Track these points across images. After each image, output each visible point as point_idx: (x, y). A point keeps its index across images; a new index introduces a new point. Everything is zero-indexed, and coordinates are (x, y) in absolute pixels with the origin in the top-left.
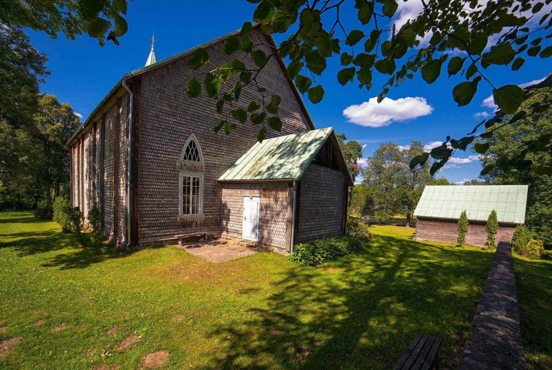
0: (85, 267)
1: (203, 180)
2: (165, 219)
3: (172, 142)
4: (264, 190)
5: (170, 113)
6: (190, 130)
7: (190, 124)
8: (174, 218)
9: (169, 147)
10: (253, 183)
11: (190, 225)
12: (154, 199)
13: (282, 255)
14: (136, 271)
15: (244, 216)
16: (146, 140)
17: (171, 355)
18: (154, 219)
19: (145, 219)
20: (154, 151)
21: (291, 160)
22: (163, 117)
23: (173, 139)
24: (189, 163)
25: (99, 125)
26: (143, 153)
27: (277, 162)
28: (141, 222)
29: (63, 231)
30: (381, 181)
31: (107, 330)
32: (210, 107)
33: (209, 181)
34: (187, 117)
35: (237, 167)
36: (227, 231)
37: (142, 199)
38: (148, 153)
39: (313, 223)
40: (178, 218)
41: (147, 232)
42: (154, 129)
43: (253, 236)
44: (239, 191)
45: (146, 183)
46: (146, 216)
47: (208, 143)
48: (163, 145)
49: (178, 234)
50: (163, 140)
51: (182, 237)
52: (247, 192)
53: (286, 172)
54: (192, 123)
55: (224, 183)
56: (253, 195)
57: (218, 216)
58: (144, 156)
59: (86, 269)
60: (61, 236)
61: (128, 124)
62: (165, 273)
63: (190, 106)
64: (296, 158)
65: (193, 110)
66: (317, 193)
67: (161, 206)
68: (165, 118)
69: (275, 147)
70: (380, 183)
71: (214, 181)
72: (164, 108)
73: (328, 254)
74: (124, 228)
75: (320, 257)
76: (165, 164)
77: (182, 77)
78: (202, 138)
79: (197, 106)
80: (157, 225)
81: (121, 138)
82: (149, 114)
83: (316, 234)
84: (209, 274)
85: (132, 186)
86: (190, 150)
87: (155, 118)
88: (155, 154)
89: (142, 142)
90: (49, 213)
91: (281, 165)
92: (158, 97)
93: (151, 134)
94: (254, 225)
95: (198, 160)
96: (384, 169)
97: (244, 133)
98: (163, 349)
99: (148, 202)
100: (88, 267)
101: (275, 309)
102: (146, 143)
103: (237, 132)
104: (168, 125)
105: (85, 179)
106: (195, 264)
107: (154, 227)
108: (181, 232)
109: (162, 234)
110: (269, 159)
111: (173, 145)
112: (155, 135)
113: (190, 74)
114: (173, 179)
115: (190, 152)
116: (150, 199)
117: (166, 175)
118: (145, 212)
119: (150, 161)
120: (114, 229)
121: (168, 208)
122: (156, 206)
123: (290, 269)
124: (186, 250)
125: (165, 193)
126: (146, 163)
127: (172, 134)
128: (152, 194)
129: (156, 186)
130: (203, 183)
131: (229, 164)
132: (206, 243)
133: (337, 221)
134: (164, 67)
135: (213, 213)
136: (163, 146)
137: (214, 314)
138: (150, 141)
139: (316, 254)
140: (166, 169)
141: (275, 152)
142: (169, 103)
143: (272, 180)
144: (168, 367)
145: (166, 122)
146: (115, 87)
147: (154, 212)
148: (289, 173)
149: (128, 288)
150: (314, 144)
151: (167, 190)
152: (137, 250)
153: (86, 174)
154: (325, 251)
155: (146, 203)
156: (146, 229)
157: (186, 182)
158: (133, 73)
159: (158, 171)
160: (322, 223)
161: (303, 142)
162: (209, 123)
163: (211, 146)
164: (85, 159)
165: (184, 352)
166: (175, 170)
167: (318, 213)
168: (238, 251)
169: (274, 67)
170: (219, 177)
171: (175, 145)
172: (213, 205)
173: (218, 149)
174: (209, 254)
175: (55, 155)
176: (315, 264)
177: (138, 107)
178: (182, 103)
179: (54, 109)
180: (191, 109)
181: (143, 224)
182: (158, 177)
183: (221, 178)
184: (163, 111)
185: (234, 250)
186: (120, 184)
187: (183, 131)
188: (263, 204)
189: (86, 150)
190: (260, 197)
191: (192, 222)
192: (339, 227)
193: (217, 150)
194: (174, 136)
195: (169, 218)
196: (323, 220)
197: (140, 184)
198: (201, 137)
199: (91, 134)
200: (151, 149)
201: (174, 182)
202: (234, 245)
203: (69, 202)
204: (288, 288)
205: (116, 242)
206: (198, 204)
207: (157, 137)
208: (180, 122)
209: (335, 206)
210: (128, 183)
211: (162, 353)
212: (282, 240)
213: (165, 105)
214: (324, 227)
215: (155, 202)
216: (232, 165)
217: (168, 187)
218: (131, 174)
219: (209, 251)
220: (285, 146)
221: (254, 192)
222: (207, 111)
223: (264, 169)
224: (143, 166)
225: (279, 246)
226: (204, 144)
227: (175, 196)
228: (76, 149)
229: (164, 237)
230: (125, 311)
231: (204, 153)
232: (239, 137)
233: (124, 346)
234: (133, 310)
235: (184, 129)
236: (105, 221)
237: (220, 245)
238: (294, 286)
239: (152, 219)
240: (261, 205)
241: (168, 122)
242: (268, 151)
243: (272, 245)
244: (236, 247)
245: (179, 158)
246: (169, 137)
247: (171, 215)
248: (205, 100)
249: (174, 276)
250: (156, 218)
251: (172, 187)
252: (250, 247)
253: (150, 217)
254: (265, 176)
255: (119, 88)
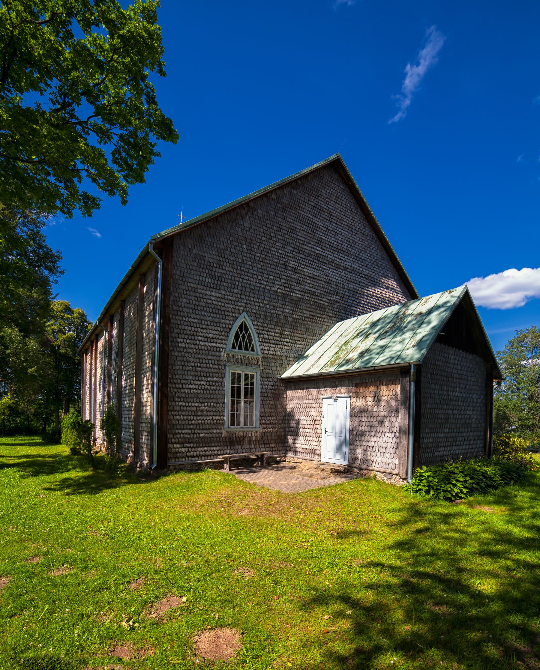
0: (96, 494)
1: (259, 378)
2: (206, 432)
3: (215, 325)
4: (357, 385)
5: (212, 285)
6: (240, 308)
7: (240, 300)
8: (218, 431)
9: (211, 331)
10: (338, 378)
11: (240, 441)
12: (190, 404)
13: (391, 484)
14: (167, 501)
15: (323, 427)
16: (179, 322)
17: (246, 637)
18: (189, 431)
19: (177, 431)
20: (190, 337)
21: (398, 339)
22: (203, 292)
23: (216, 320)
24: (240, 354)
25: (117, 317)
26: (175, 340)
27: (375, 345)
28: (172, 436)
29: (72, 453)
30: (521, 386)
31: (129, 582)
32: (267, 276)
33: (269, 380)
34: (235, 291)
35: (309, 359)
36: (295, 452)
37: (173, 404)
38: (182, 340)
39: (440, 435)
40: (224, 432)
41: (180, 449)
42: (190, 307)
43: (338, 456)
44: (314, 392)
45: (179, 381)
46: (178, 427)
47: (266, 325)
48: (203, 328)
49: (224, 454)
50: (203, 322)
51: (230, 458)
52: (328, 392)
53: (393, 356)
54: (243, 299)
55: (291, 382)
56: (338, 395)
57: (281, 430)
58: (177, 345)
59: (99, 496)
60: (68, 458)
61: (155, 302)
62: (211, 505)
63: (239, 276)
64: (408, 335)
65: (244, 281)
66: (445, 388)
67: (200, 413)
68: (205, 292)
69: (368, 326)
70: (518, 389)
71: (275, 380)
72: (204, 279)
73: (473, 483)
74: (147, 445)
75: (461, 486)
76: (206, 355)
77: (228, 237)
78: (258, 319)
79: (249, 275)
80: (194, 441)
81: (145, 325)
82: (184, 287)
83: (445, 453)
84: (279, 509)
85: (160, 384)
86: (241, 336)
87: (191, 293)
88: (192, 342)
89: (174, 325)
90: (57, 436)
91: (383, 348)
92: (196, 265)
93: (186, 314)
94: (340, 440)
95: (253, 350)
96: (524, 367)
97: (317, 311)
98: (229, 625)
99: (182, 408)
100: (101, 494)
101: (413, 565)
102: (180, 326)
103: (306, 310)
104: (209, 301)
105: (98, 389)
106: (254, 495)
107: (190, 443)
108: (228, 451)
109: (201, 453)
110: (362, 341)
111: (216, 328)
112: (192, 316)
113: (238, 233)
114: (217, 375)
115: (241, 338)
116: (184, 404)
117: (206, 370)
118: (177, 422)
119: (185, 350)
120: (135, 448)
121: (209, 416)
122: (193, 414)
123: (411, 504)
124: (237, 476)
125: (206, 396)
126: (180, 354)
127: (216, 313)
128: (187, 396)
129: (194, 386)
130: (259, 382)
131: (296, 355)
132: (265, 467)
133: (477, 433)
134: (203, 225)
135: (275, 426)
136: (202, 331)
137: (309, 568)
138: (185, 324)
139: (454, 482)
140: (207, 361)
141: (370, 332)
142: (210, 272)
143: (372, 369)
144: (246, 662)
145: (207, 297)
146: (139, 257)
147: (190, 422)
148: (399, 357)
149: (157, 523)
150: (435, 313)
151: (208, 392)
152: (165, 475)
153: (100, 383)
154: (468, 478)
155: (179, 409)
156: (178, 446)
157: (236, 378)
158: (163, 233)
159: (196, 364)
160: (454, 435)
161: (416, 312)
162: (266, 298)
163: (270, 330)
164: (99, 365)
165: (269, 636)
166: (219, 363)
167: (447, 419)
168: (319, 477)
169: (356, 219)
170: (283, 374)
171: (219, 329)
172: (274, 414)
173: (281, 334)
174: (273, 481)
175: (65, 369)
176: (453, 499)
177: (169, 279)
178: (228, 272)
179: (66, 316)
180: (241, 280)
181: (175, 439)
182: (196, 374)
183: (287, 374)
184: (203, 284)
185: (311, 476)
186: (143, 386)
187: (230, 309)
188: (355, 407)
189: (100, 352)
190: (350, 397)
191: (244, 438)
192: (480, 444)
193: (278, 335)
194: (218, 316)
195: (211, 431)
196: (455, 430)
197: (171, 382)
198: (255, 317)
199: (106, 332)
200: (187, 334)
201: (218, 380)
202: (310, 470)
203: (79, 416)
204: (419, 531)
205: (137, 465)
206: (253, 412)
207: (194, 318)
208: (226, 297)
209: (473, 410)
210: (155, 381)
211: (229, 632)
212: (391, 460)
213: (205, 275)
214: (458, 443)
215: (192, 408)
216: (301, 356)
217: (209, 387)
218: (160, 369)
219: (271, 478)
220: (383, 322)
221: (339, 390)
222: (262, 282)
223: (354, 355)
224: (175, 358)
225: (387, 470)
226: (260, 328)
227: (220, 399)
228: (89, 354)
229: (203, 458)
230: (155, 556)
231: (261, 339)
232: (310, 317)
233: (158, 612)
234: (169, 555)
235: (232, 306)
236: (122, 439)
237: (287, 471)
238: (427, 529)
239: (187, 431)
240: (352, 409)
241: (209, 297)
242: (358, 332)
243: (372, 468)
244: (313, 472)
245: (225, 346)
246: (211, 319)
247: (214, 427)
248: (260, 267)
249: (225, 510)
250: (193, 431)
251: (215, 388)
252: (337, 472)
253: (184, 429)
254: (358, 365)
255: (145, 255)
